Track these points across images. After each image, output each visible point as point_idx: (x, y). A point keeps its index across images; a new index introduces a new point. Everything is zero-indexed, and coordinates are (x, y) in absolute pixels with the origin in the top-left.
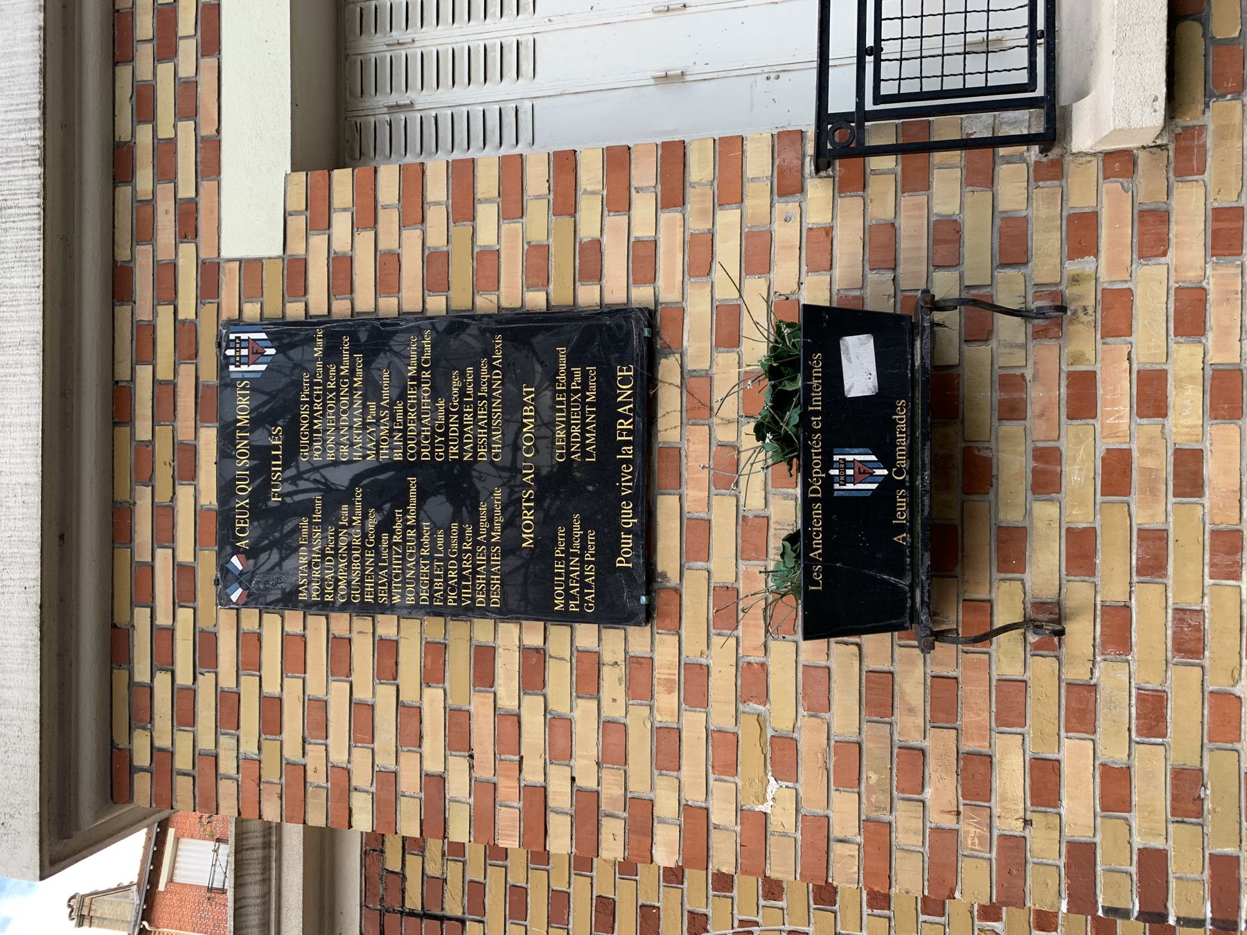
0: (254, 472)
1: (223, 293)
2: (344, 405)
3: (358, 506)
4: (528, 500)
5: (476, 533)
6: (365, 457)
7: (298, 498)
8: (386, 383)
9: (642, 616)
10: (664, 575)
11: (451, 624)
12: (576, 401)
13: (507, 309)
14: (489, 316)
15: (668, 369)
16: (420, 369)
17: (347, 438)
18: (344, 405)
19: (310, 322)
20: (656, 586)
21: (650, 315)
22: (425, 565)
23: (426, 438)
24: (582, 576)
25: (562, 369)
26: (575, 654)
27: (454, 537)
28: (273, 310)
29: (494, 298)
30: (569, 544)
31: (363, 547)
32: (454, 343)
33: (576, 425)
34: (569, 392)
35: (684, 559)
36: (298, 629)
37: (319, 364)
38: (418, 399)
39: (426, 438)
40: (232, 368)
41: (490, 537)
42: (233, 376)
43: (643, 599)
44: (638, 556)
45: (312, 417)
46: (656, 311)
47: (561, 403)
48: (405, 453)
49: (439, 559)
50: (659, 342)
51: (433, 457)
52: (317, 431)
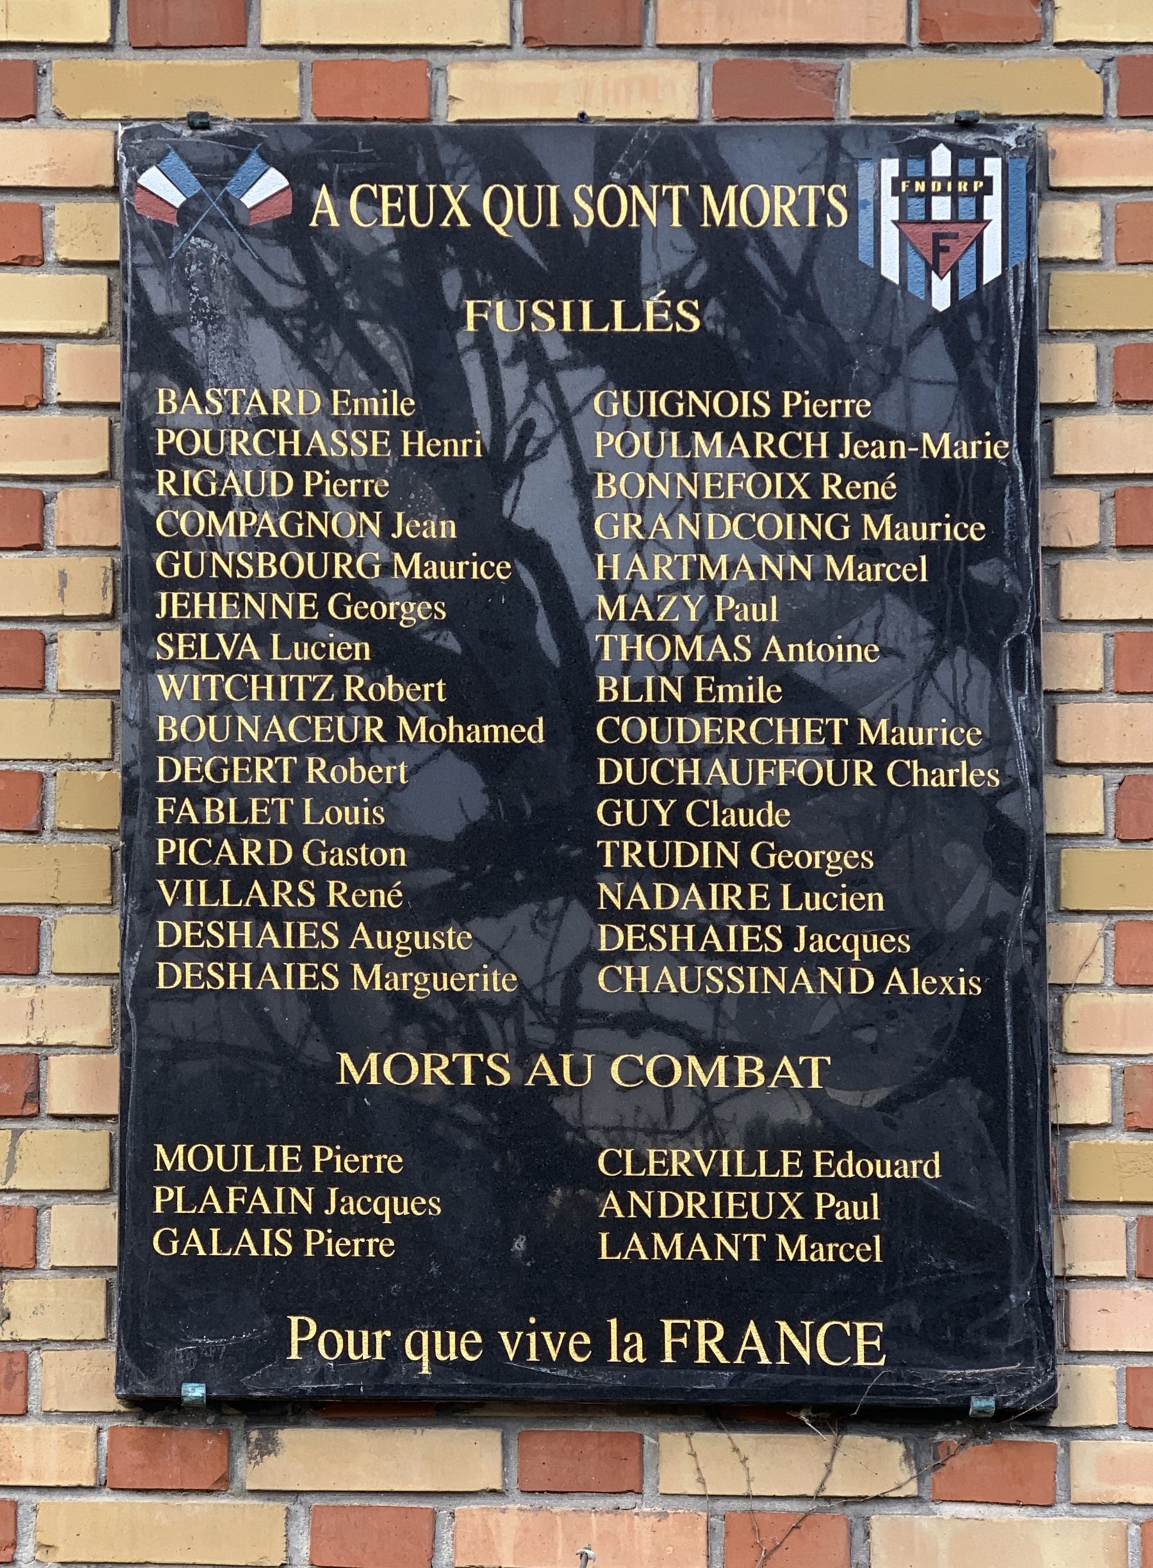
0: (559, 241)
1: (1135, 135)
2: (770, 526)
3: (455, 571)
4: (480, 1069)
5: (378, 920)
6: (610, 589)
7: (473, 366)
8: (837, 653)
9: (147, 1388)
10: (267, 1447)
11: (101, 848)
12: (780, 1205)
13: (1059, 1010)
14: (1039, 950)
15: (873, 1462)
16: (881, 755)
17: (661, 520)
18: (770, 526)
19: (1031, 419)
20: (236, 1425)
21: (1034, 1414)
22: (277, 771)
23: (667, 772)
24: (257, 1222)
25: (875, 1168)
26: (29, 1203)
27: (364, 856)
28: (1073, 301)
29: (1094, 974)
30: (352, 1185)
31: (327, 586)
32: (960, 855)
33: (709, 1207)
34: (807, 1186)
35: (316, 1502)
36: (62, 387)
37: (899, 449)
38: (787, 750)
39: (667, 772)
40: (890, 168)
41: (367, 959)
42: (864, 171)
43: (195, 1391)
44: (321, 1376)
45: (729, 427)
46: (1046, 1430)
47: (774, 1163)
48: (621, 709)
49: (295, 812)
50: (953, 1439)
51: (605, 792)
52: (686, 444)
